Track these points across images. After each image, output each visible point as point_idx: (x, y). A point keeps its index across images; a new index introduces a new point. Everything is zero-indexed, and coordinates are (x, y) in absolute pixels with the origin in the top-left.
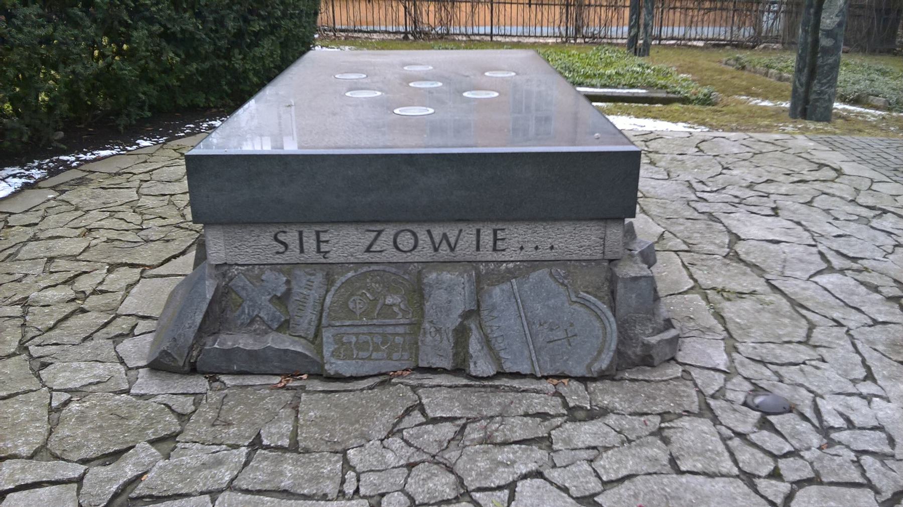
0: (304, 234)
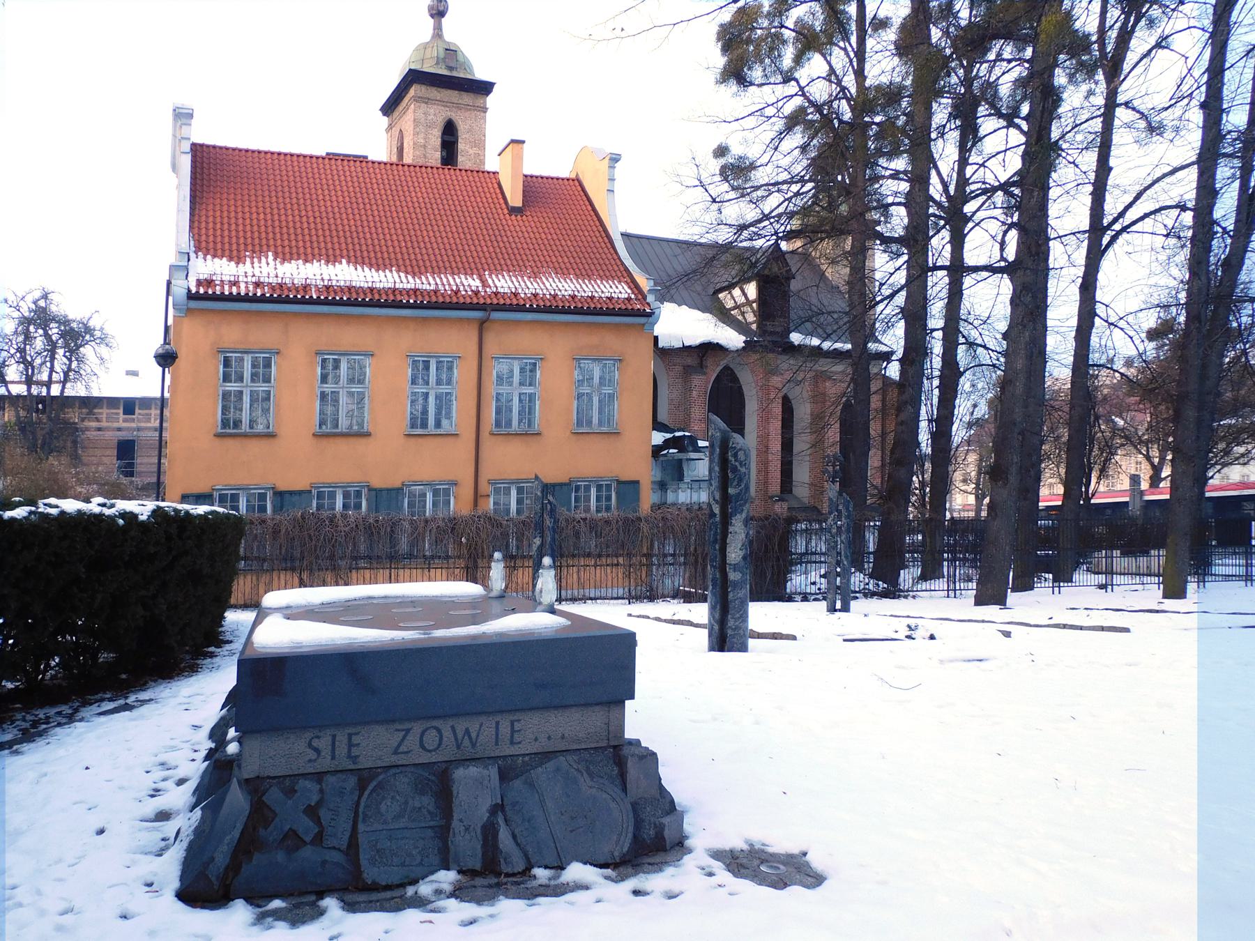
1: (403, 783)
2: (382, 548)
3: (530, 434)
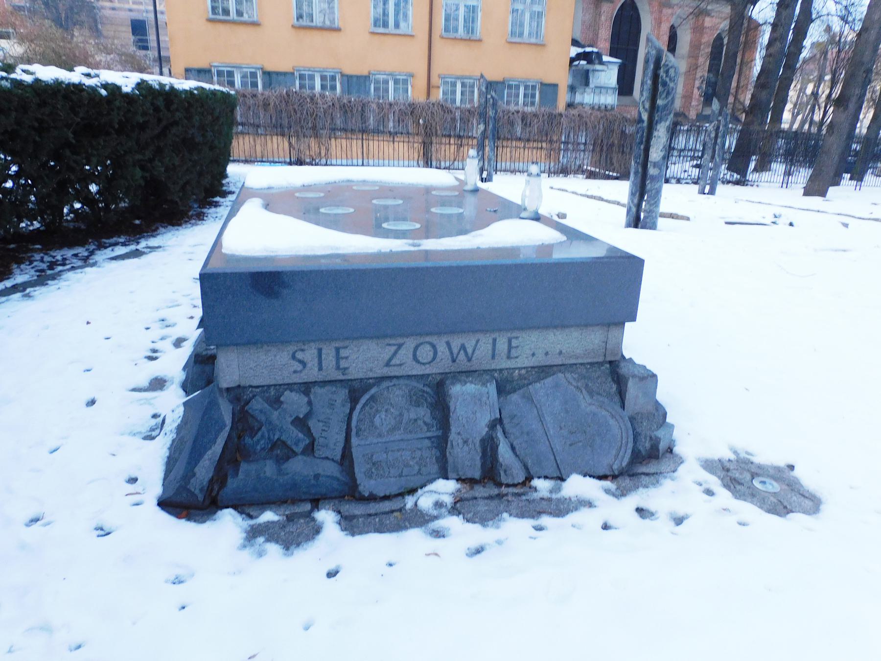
0: (324, 351)
1: (397, 395)
2: (355, 122)
3: (471, 39)
